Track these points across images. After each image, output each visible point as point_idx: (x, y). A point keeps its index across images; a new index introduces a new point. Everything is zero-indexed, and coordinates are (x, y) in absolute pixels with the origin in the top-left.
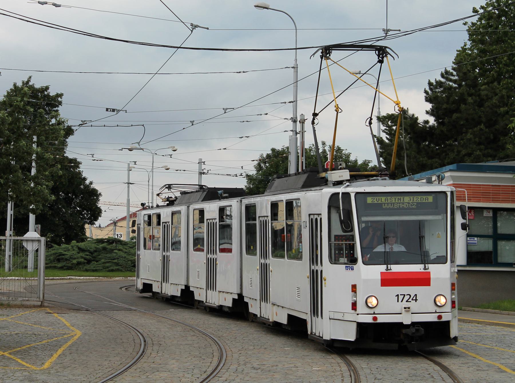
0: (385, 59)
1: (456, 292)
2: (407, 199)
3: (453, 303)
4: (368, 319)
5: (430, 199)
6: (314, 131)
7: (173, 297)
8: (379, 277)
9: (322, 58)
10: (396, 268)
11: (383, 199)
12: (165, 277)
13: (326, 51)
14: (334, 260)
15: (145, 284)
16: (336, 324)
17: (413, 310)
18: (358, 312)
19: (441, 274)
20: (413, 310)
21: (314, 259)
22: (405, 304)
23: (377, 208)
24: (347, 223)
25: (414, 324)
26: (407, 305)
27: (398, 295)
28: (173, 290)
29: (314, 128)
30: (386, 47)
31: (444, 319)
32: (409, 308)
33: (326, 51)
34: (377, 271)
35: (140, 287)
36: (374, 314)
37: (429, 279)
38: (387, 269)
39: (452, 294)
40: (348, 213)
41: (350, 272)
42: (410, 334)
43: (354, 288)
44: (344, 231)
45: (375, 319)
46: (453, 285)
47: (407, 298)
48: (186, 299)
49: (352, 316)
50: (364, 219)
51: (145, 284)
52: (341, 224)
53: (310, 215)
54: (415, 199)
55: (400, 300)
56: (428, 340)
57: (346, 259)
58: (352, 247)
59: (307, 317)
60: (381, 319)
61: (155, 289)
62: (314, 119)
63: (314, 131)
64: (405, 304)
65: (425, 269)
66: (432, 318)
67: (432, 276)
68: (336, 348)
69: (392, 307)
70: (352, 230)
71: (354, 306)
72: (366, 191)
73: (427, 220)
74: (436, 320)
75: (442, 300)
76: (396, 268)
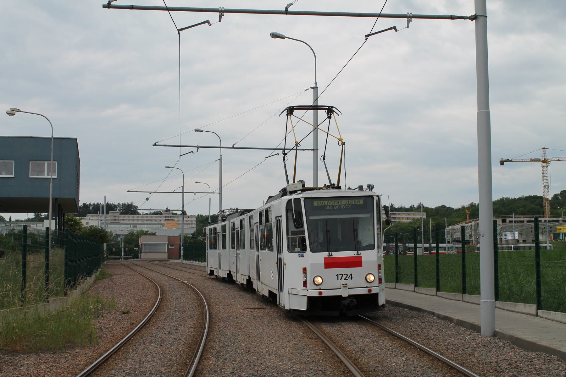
0: (332, 115)
1: (382, 271)
2: (344, 202)
3: (380, 280)
4: (315, 294)
5: (361, 202)
6: (285, 165)
7: (224, 278)
8: (323, 262)
9: (287, 116)
10: (336, 254)
11: (326, 202)
12: (219, 267)
13: (290, 111)
14: (291, 249)
15: (211, 270)
16: (294, 299)
17: (349, 286)
18: (308, 288)
19: (371, 257)
20: (349, 286)
21: (279, 250)
22: (343, 281)
23: (322, 210)
24: (298, 222)
25: (350, 296)
26: (345, 282)
27: (338, 275)
28: (223, 274)
29: (284, 163)
30: (332, 107)
31: (373, 292)
32: (346, 284)
33: (290, 111)
34: (321, 257)
35: (209, 272)
36: (320, 289)
37: (361, 262)
38: (329, 255)
39: (379, 273)
40: (299, 214)
41: (302, 258)
42: (346, 304)
43: (305, 270)
44: (296, 227)
45: (320, 293)
46: (380, 266)
47: (344, 276)
48: (229, 280)
49: (304, 292)
50: (311, 218)
51: (211, 270)
52: (294, 222)
53: (276, 217)
54: (350, 202)
55: (340, 278)
56: (361, 309)
57: (53, 221)
58: (303, 240)
59: (276, 292)
60: (325, 293)
61: (215, 273)
62: (284, 157)
63: (285, 165)
64: (343, 281)
65: (358, 254)
66: (364, 291)
67: (364, 260)
68: (293, 315)
69: (333, 284)
70: (302, 226)
71: (305, 284)
72: (313, 196)
73: (359, 218)
74: (367, 293)
75: (371, 278)
76: (336, 254)
